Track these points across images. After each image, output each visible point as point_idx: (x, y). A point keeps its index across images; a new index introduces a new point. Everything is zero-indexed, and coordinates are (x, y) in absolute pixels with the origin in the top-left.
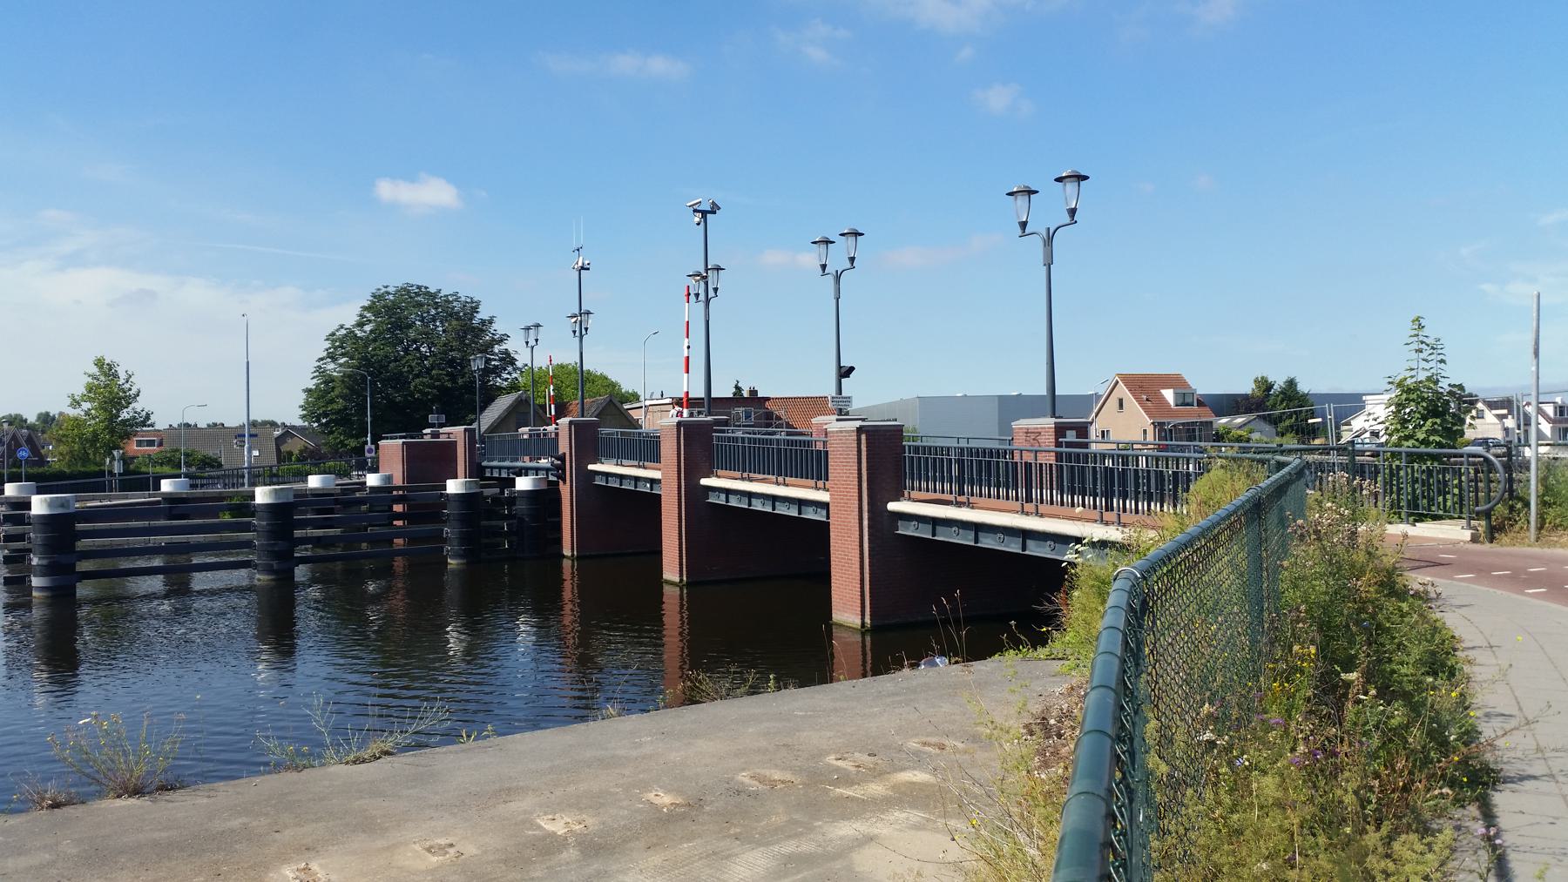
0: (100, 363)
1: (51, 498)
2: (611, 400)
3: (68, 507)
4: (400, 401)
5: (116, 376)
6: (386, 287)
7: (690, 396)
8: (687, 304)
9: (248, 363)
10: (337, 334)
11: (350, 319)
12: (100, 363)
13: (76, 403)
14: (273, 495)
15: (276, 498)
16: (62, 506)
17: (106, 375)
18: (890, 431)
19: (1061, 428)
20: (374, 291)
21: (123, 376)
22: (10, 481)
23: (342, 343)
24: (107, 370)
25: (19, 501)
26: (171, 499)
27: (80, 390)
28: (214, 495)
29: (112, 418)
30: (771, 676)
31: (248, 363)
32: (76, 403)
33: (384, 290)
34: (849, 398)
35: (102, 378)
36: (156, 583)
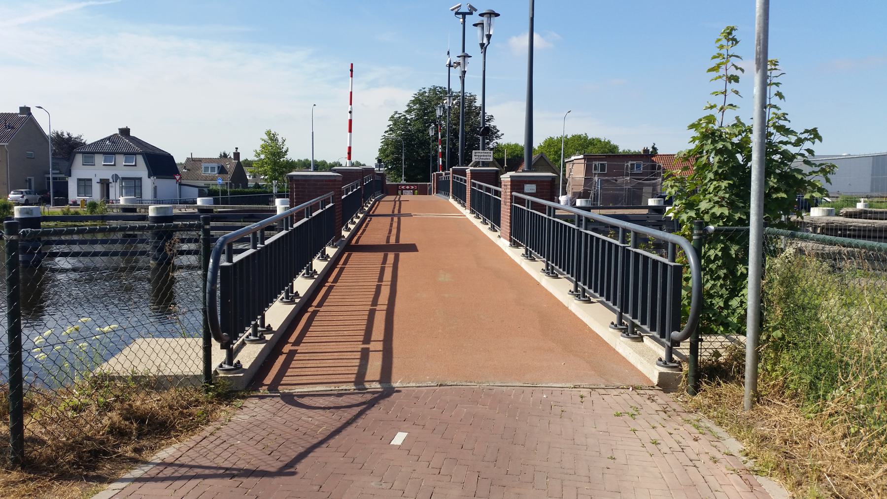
0: (268, 133)
1: (21, 208)
2: (542, 156)
3: (32, 214)
4: (424, 156)
5: (277, 140)
6: (424, 88)
7: (242, 159)
8: (350, 106)
9: (313, 133)
10: (395, 117)
11: (402, 109)
12: (268, 133)
13: (258, 155)
14: (156, 211)
15: (157, 213)
16: (27, 213)
17: (271, 139)
18: (322, 181)
19: (518, 181)
20: (418, 91)
21: (280, 140)
22: (278, 198)
23: (397, 122)
24: (273, 138)
25: (129, 207)
26: (202, 210)
27: (259, 149)
28: (247, 209)
29: (275, 163)
30: (700, 337)
31: (313, 133)
32: (258, 155)
33: (423, 90)
34: (83, 165)
35: (270, 142)
36: (193, 260)
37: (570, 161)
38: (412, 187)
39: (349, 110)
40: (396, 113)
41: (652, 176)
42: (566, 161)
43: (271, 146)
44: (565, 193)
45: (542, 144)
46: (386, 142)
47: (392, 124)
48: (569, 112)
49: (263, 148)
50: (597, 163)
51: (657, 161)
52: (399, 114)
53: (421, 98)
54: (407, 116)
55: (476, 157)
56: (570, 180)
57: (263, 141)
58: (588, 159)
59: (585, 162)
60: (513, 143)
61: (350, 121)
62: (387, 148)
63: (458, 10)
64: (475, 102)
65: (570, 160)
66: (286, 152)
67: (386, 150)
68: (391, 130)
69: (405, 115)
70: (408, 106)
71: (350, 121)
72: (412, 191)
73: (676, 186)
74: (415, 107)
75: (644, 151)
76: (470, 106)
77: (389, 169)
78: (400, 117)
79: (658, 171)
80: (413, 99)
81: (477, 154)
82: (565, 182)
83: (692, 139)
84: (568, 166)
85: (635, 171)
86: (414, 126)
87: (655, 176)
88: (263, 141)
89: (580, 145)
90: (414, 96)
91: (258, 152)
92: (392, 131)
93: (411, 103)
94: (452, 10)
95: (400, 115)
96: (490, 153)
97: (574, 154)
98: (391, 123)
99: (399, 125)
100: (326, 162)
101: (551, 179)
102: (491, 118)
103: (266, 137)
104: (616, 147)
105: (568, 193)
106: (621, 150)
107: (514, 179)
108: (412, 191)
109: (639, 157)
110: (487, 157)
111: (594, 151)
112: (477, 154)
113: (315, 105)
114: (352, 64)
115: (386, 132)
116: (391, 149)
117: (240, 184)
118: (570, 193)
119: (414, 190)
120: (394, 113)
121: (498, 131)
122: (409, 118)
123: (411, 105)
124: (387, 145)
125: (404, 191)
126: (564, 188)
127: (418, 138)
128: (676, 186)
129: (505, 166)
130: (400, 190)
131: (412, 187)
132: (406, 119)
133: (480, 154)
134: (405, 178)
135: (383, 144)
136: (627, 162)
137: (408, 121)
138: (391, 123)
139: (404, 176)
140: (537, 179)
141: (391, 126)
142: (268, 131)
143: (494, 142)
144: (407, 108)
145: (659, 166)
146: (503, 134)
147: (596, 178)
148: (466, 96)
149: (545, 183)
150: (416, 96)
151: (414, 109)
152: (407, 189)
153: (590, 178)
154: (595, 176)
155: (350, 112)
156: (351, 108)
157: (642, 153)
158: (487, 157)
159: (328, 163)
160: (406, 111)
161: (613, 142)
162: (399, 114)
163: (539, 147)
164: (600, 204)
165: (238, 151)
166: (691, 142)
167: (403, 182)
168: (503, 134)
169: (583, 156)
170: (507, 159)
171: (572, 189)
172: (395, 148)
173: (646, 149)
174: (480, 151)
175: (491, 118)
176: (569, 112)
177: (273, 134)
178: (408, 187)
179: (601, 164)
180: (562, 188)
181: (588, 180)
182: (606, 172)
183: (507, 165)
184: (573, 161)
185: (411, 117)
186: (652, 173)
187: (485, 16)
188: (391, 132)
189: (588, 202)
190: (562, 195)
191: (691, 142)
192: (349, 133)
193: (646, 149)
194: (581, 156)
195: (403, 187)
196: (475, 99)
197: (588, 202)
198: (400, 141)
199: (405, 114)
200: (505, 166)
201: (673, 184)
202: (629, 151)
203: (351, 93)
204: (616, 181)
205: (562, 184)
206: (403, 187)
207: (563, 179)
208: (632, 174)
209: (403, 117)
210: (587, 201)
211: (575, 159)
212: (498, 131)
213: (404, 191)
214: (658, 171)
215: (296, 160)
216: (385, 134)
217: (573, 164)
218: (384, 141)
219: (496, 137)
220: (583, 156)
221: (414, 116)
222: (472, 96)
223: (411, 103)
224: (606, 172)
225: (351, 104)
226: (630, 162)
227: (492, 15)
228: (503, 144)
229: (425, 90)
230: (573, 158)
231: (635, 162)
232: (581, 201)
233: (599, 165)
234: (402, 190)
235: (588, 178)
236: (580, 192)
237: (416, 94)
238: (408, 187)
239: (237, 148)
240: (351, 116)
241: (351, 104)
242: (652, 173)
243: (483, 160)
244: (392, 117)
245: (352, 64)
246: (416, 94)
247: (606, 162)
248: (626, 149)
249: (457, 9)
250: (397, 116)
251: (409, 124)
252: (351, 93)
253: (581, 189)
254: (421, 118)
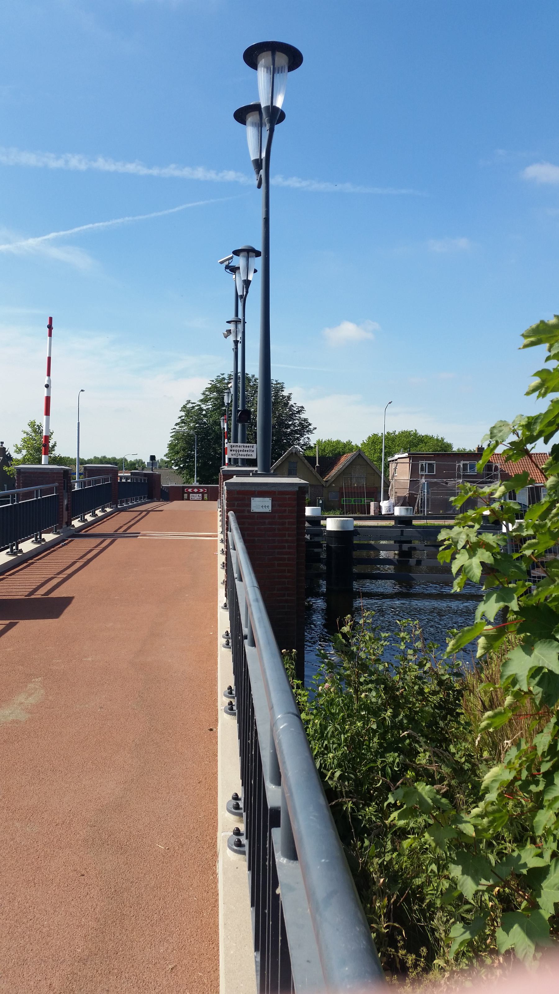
6: (223, 374)
9: (79, 423)
11: (196, 397)
17: (35, 431)
19: (239, 492)
20: (216, 378)
31: (79, 423)
33: (222, 376)
35: (33, 434)
37: (393, 461)
38: (201, 490)
39: (46, 383)
40: (189, 402)
41: (488, 478)
42: (389, 460)
43: (35, 440)
44: (387, 498)
45: (365, 442)
46: (177, 436)
47: (184, 415)
48: (390, 403)
49: (25, 442)
50: (424, 462)
51: (493, 461)
52: (193, 403)
53: (218, 385)
54: (203, 406)
55: (233, 453)
56: (392, 482)
57: (25, 434)
58: (414, 458)
59: (410, 461)
60: (334, 439)
61: (48, 399)
62: (178, 443)
63: (229, 263)
64: (283, 391)
65: (393, 459)
66: (54, 446)
67: (175, 445)
68: (183, 422)
69: (200, 405)
70: (204, 394)
71: (48, 399)
72: (200, 495)
73: (488, 547)
74: (212, 396)
75: (478, 449)
76: (276, 395)
77: (180, 468)
78: (193, 407)
79: (495, 473)
80: (210, 386)
81: (233, 449)
82: (387, 484)
83: (537, 381)
84: (392, 466)
85: (469, 472)
86: (211, 417)
87: (491, 478)
88: (25, 434)
89: (409, 442)
90: (210, 382)
91: (19, 446)
92: (185, 423)
93: (206, 391)
94: (222, 263)
95: (194, 405)
96: (253, 447)
97: (398, 452)
98: (183, 414)
99: (192, 416)
100: (126, 460)
101: (297, 489)
102: (301, 410)
103: (29, 430)
104: (449, 446)
105: (391, 498)
106: (455, 449)
107: (232, 488)
108: (200, 495)
109: (473, 456)
110: (249, 453)
111: (423, 449)
112: (233, 449)
113: (82, 391)
114: (51, 319)
115: (177, 424)
116: (182, 444)
117: (6, 485)
118: (393, 497)
119: (203, 493)
120: (186, 403)
121: (310, 425)
122: (205, 408)
123: (207, 393)
124: (177, 439)
125: (191, 495)
126: (386, 492)
127: (214, 431)
128: (488, 547)
129: (317, 465)
130: (186, 493)
131: (201, 490)
132: (201, 409)
133: (238, 449)
134: (198, 478)
135: (173, 439)
136: (459, 462)
137: (204, 412)
138: (183, 414)
139: (197, 477)
140: (273, 489)
141: (183, 418)
142: (32, 422)
143: (305, 437)
144: (202, 397)
145: (496, 468)
146: (316, 428)
147: (423, 480)
148: (272, 383)
149: (287, 496)
150: (213, 383)
151: (211, 398)
152: (194, 493)
153: (417, 480)
154: (421, 478)
155: (47, 386)
156: (49, 381)
157: (476, 452)
158: (249, 453)
159: (129, 461)
160: (201, 401)
161: (447, 440)
162: (193, 403)
163: (362, 445)
164: (427, 511)
165: (4, 446)
166: (534, 390)
167: (195, 484)
168: (316, 428)
169: (407, 454)
170: (319, 457)
171: (396, 493)
172: (186, 443)
173: (480, 447)
174: (239, 444)
175: (301, 410)
176: (390, 403)
177: (38, 426)
178: (196, 490)
179: (429, 464)
180: (384, 492)
181: (414, 483)
182: (435, 473)
183: (318, 464)
184: (396, 460)
185: (207, 407)
186: (488, 474)
187: (242, 254)
188: (183, 424)
189: (409, 510)
190: (384, 500)
191: (534, 390)
192: (45, 416)
193: (480, 447)
194: (406, 455)
195: (190, 490)
196: (282, 388)
197: (409, 510)
198: (192, 436)
199: (200, 403)
200: (317, 465)
201: (474, 539)
202: (465, 450)
203: (49, 359)
204: (447, 483)
205: (384, 487)
206: (190, 490)
207: (384, 481)
208: (465, 476)
209: (197, 408)
210: (407, 509)
211: (399, 458)
212: (310, 425)
213: (191, 495)
214: (495, 473)
215: (92, 458)
216: (175, 427)
217: (397, 463)
218: (175, 435)
219: (308, 431)
220: (407, 454)
221: (211, 406)
222: (279, 384)
223: (206, 391)
224: (435, 473)
225: (49, 375)
226: (462, 462)
227: (251, 254)
228: (323, 441)
229: (224, 376)
230: (396, 456)
231: (468, 462)
232: (400, 509)
233: (427, 464)
234: (189, 493)
235: (414, 480)
236: (405, 497)
237: (213, 381)
238: (196, 490)
239: (2, 443)
240: (49, 392)
241: (49, 375)
242: (488, 474)
243: (243, 457)
244: (184, 407)
245: (51, 319)
246: (213, 381)
247: (435, 462)
248: (461, 448)
249: (227, 262)
250: (190, 405)
251: (205, 416)
252: (49, 359)
253: (405, 493)
254: (219, 408)
